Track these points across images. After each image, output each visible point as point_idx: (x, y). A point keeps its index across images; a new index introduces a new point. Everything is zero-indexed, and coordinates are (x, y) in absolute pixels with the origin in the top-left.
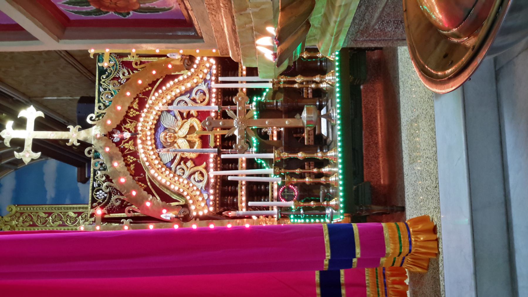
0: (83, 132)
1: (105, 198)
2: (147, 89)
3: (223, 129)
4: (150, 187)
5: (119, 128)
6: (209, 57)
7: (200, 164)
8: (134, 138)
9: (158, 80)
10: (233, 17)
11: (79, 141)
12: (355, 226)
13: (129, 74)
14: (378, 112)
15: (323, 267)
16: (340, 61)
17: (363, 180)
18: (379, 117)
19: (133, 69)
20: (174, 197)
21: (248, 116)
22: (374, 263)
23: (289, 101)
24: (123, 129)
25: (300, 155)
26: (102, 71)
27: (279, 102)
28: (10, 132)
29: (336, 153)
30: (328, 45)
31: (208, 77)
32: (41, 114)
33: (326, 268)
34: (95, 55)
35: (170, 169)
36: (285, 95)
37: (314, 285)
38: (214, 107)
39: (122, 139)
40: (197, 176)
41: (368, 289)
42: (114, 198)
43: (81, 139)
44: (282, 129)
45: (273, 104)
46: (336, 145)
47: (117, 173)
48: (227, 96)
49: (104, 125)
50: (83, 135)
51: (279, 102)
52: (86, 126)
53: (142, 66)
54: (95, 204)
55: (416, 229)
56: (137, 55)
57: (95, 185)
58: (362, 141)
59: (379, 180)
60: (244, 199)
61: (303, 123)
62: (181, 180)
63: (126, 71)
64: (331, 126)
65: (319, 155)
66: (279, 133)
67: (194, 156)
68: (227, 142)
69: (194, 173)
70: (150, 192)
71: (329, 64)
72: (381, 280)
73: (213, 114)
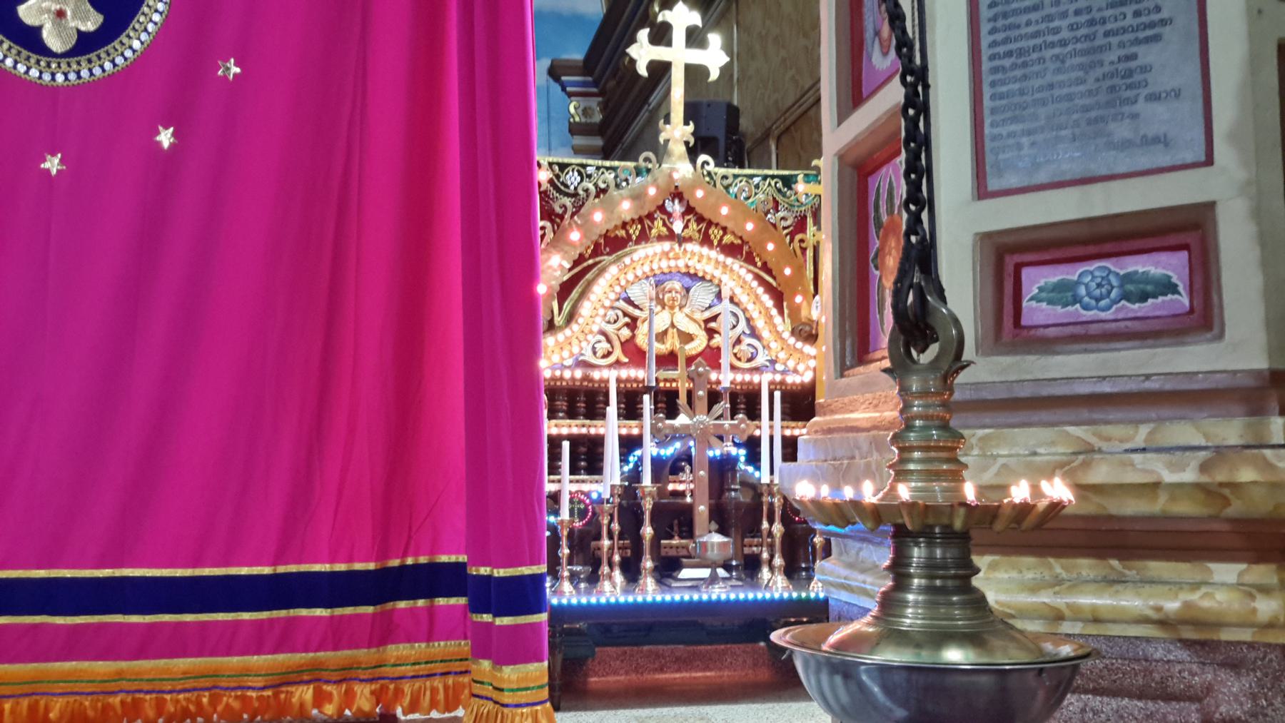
0: (683, 148)
1: (567, 186)
2: (757, 259)
3: (690, 394)
4: (585, 264)
5: (689, 210)
6: (815, 370)
7: (625, 352)
8: (671, 236)
9: (774, 278)
10: (868, 430)
11: (667, 141)
12: (543, 617)
13: (785, 228)
14: (719, 673)
15: (474, 565)
16: (808, 600)
17: (598, 645)
18: (708, 674)
19: (792, 235)
20: (567, 306)
21: (714, 440)
22: (481, 651)
23: (740, 512)
24: (687, 218)
25: (648, 531)
26: (788, 182)
27: (736, 494)
28: (682, 17)
29: (650, 592)
30: (831, 574)
31: (779, 367)
32: (714, 75)
33: (473, 571)
34: (817, 168)
35: (618, 300)
36: (748, 505)
37: (433, 552)
38: (725, 379)
39: (670, 215)
40: (604, 346)
41: (423, 645)
42: (567, 201)
43: (671, 145)
44: (689, 500)
45: (734, 482)
46: (663, 592)
47: (610, 208)
48: (746, 401)
49: (694, 185)
50: (678, 149)
51: (736, 494)
52: (692, 153)
53: (799, 252)
54: (556, 168)
55: (540, 715)
56: (818, 242)
57: (590, 170)
58: (666, 643)
59: (596, 674)
60: (575, 431)
61: (701, 536)
62: (598, 320)
63: (789, 222)
64: (696, 585)
65: (648, 564)
66: (682, 494)
67: (641, 340)
68: (668, 403)
69: (609, 341)
70: (576, 263)
71: (804, 582)
72: (440, 668)
73: (714, 376)
